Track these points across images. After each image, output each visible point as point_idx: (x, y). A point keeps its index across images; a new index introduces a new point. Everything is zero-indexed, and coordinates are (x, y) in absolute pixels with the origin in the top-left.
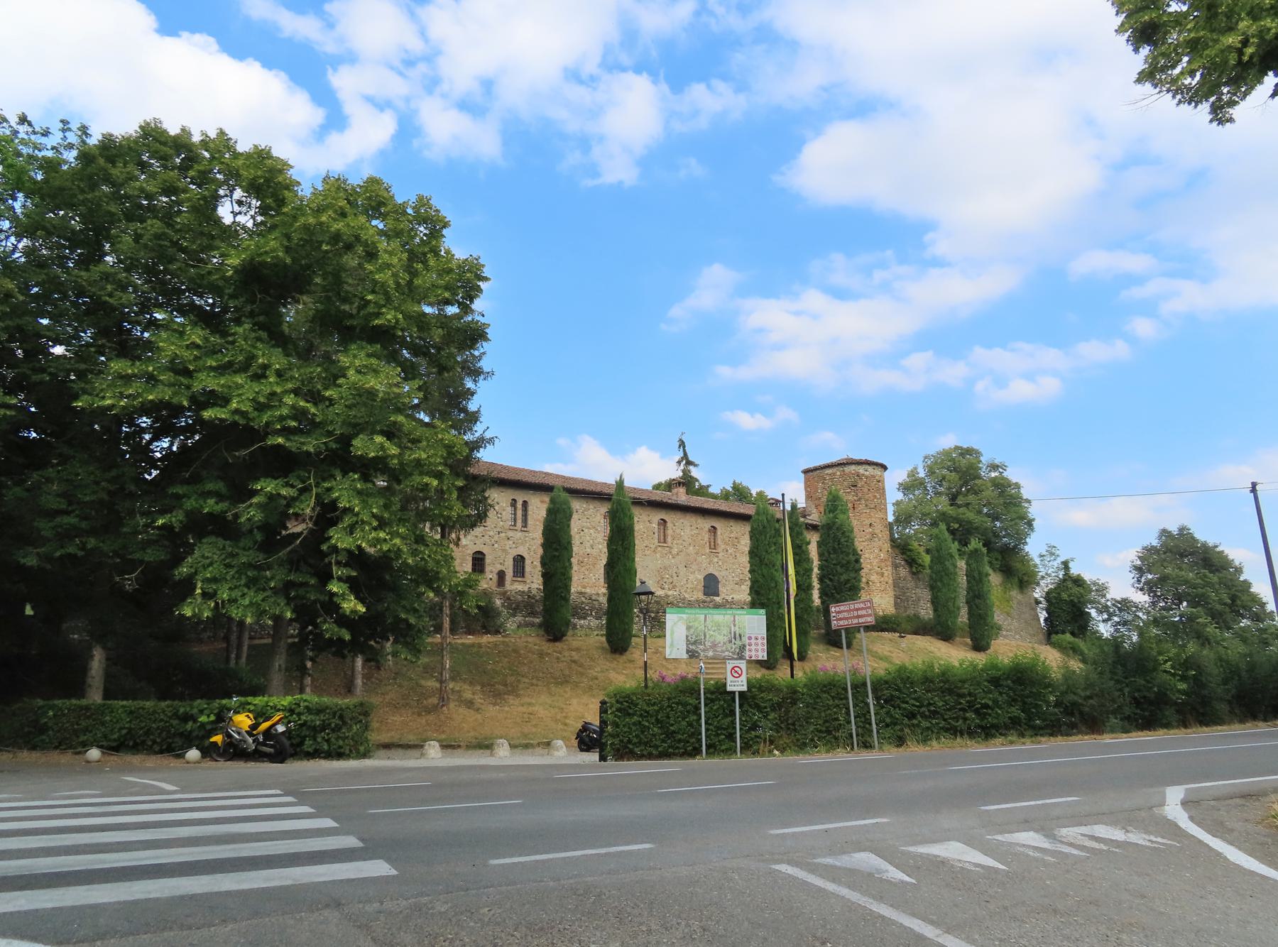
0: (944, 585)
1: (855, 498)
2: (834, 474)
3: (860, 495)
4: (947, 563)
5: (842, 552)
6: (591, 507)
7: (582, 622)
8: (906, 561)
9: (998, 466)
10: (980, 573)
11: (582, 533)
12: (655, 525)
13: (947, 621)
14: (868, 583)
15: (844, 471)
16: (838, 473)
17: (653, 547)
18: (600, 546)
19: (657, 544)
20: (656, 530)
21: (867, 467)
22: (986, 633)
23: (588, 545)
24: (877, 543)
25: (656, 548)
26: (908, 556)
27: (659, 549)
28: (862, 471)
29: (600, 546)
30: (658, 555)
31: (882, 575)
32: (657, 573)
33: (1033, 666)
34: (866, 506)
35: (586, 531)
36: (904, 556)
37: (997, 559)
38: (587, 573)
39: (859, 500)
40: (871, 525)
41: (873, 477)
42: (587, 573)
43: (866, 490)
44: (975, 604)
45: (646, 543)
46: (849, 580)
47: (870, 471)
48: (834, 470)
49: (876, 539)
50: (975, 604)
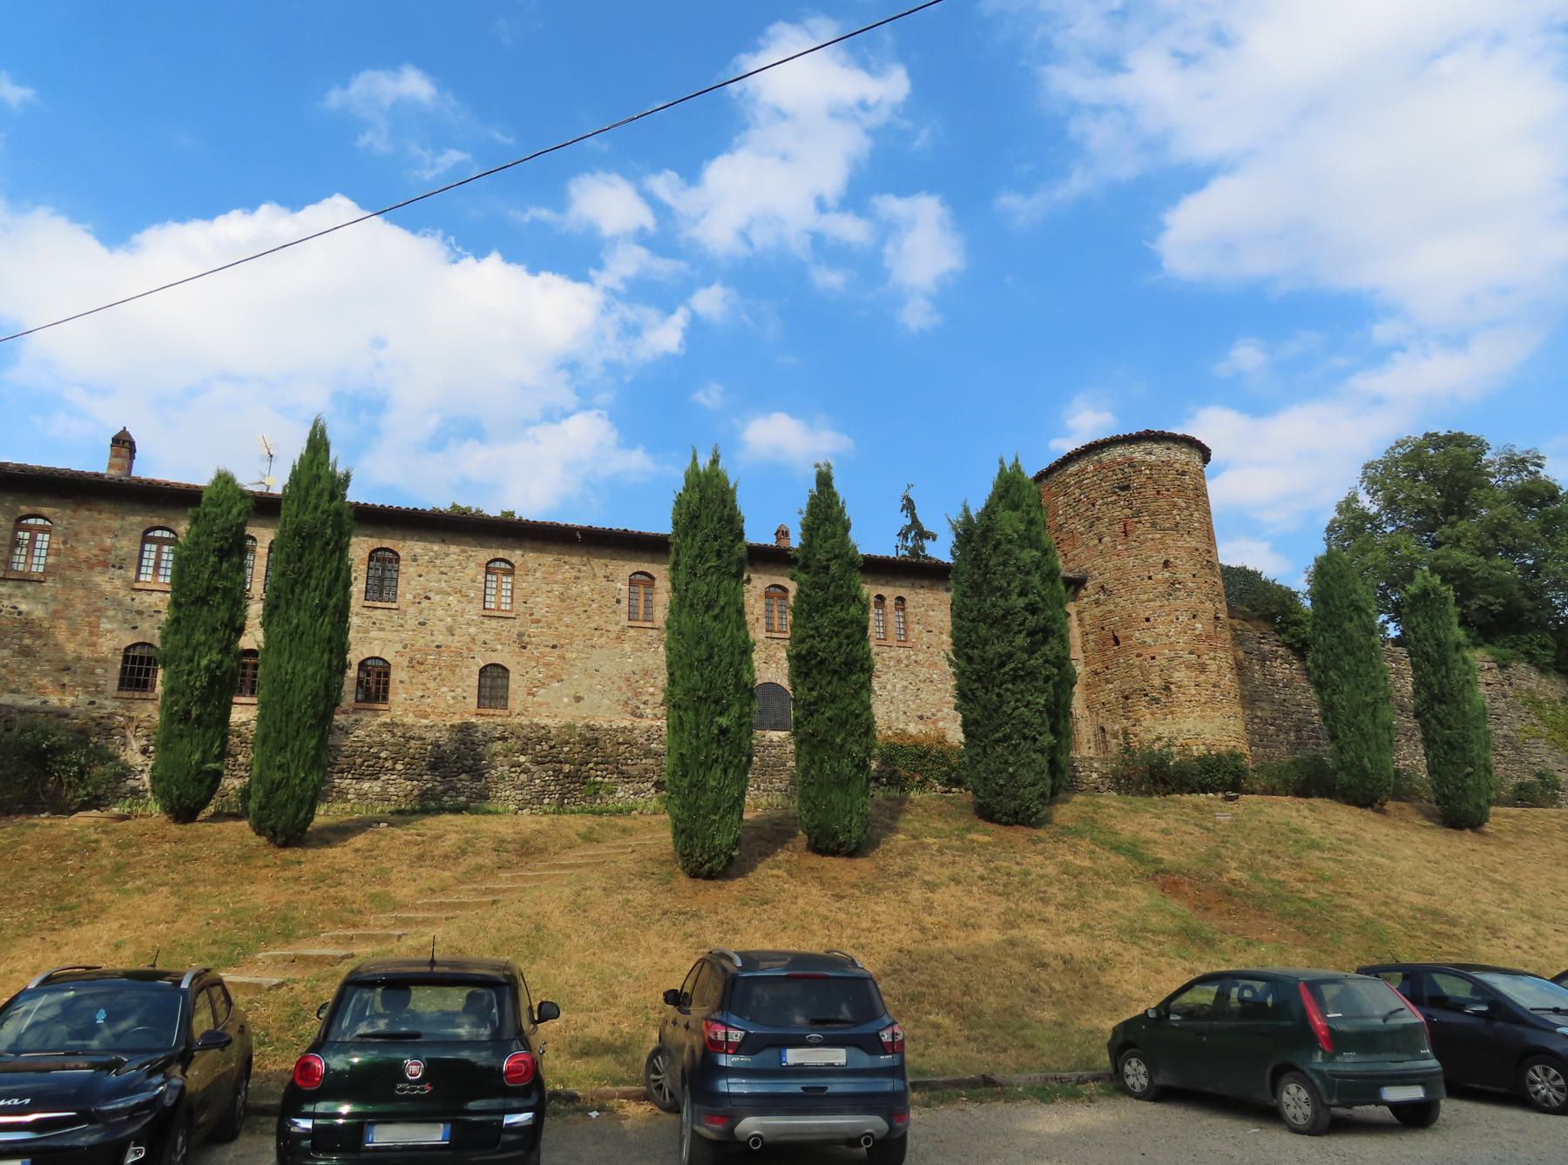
0: (1345, 676)
1: (1127, 511)
2: (1083, 471)
3: (1137, 504)
4: (1347, 625)
5: (993, 591)
6: (453, 549)
7: (366, 785)
8: (1289, 646)
9: (1523, 461)
10: (1439, 644)
11: (425, 603)
12: (622, 586)
13: (1360, 758)
14: (1167, 688)
15: (1100, 461)
16: (1091, 468)
17: (614, 629)
18: (472, 630)
19: (625, 623)
20: (624, 595)
21: (1148, 446)
22: (1470, 782)
23: (440, 626)
24: (1181, 601)
25: (623, 630)
26: (1293, 636)
27: (632, 632)
28: (1138, 456)
29: (472, 630)
30: (627, 647)
31: (1203, 669)
32: (623, 684)
33: (82, 734)
34: (1154, 525)
35: (436, 598)
36: (1284, 637)
37: (1544, 647)
38: (432, 685)
39: (1138, 513)
40: (1166, 564)
41: (1168, 464)
42: (432, 685)
43: (1150, 492)
44: (1436, 717)
45: (597, 620)
46: (1010, 656)
47: (1180, 455)
48: (1082, 464)
49: (1182, 594)
50: (1436, 717)
